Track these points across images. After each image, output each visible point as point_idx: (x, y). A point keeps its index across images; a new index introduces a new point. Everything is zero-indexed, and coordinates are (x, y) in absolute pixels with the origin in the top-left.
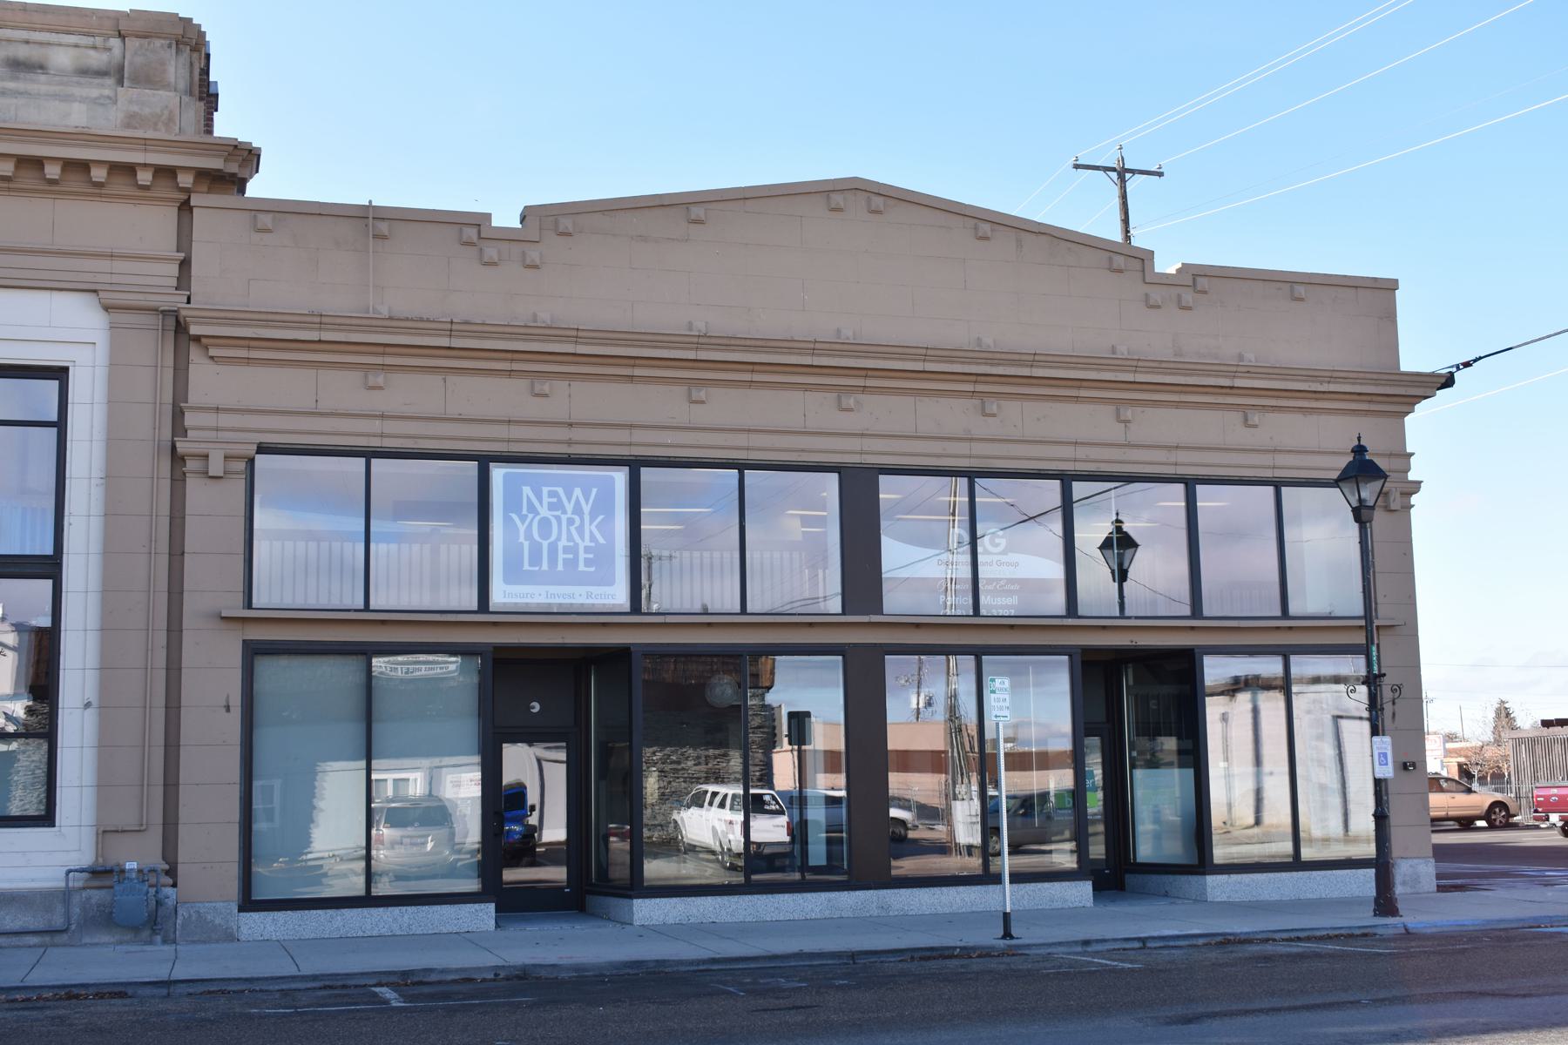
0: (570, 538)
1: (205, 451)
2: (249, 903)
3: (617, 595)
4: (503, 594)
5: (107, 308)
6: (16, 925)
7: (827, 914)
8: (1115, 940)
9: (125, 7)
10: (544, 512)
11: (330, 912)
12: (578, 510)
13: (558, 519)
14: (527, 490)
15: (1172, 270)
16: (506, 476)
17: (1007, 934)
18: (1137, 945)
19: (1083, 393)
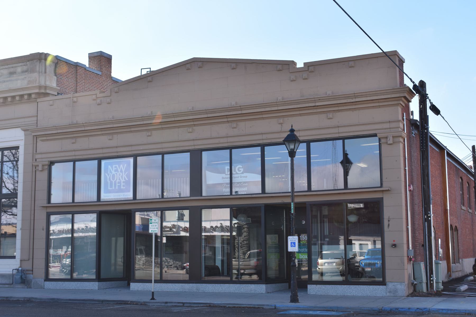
0: (119, 179)
1: (386, 136)
2: (47, 279)
3: (130, 195)
4: (105, 196)
5: (24, 130)
6: (4, 282)
7: (181, 290)
8: (175, 303)
9: (28, 53)
10: (113, 172)
11: (63, 282)
12: (121, 171)
13: (116, 174)
14: (109, 167)
15: (302, 66)
16: (105, 163)
17: (153, 299)
18: (181, 305)
19: (264, 116)
